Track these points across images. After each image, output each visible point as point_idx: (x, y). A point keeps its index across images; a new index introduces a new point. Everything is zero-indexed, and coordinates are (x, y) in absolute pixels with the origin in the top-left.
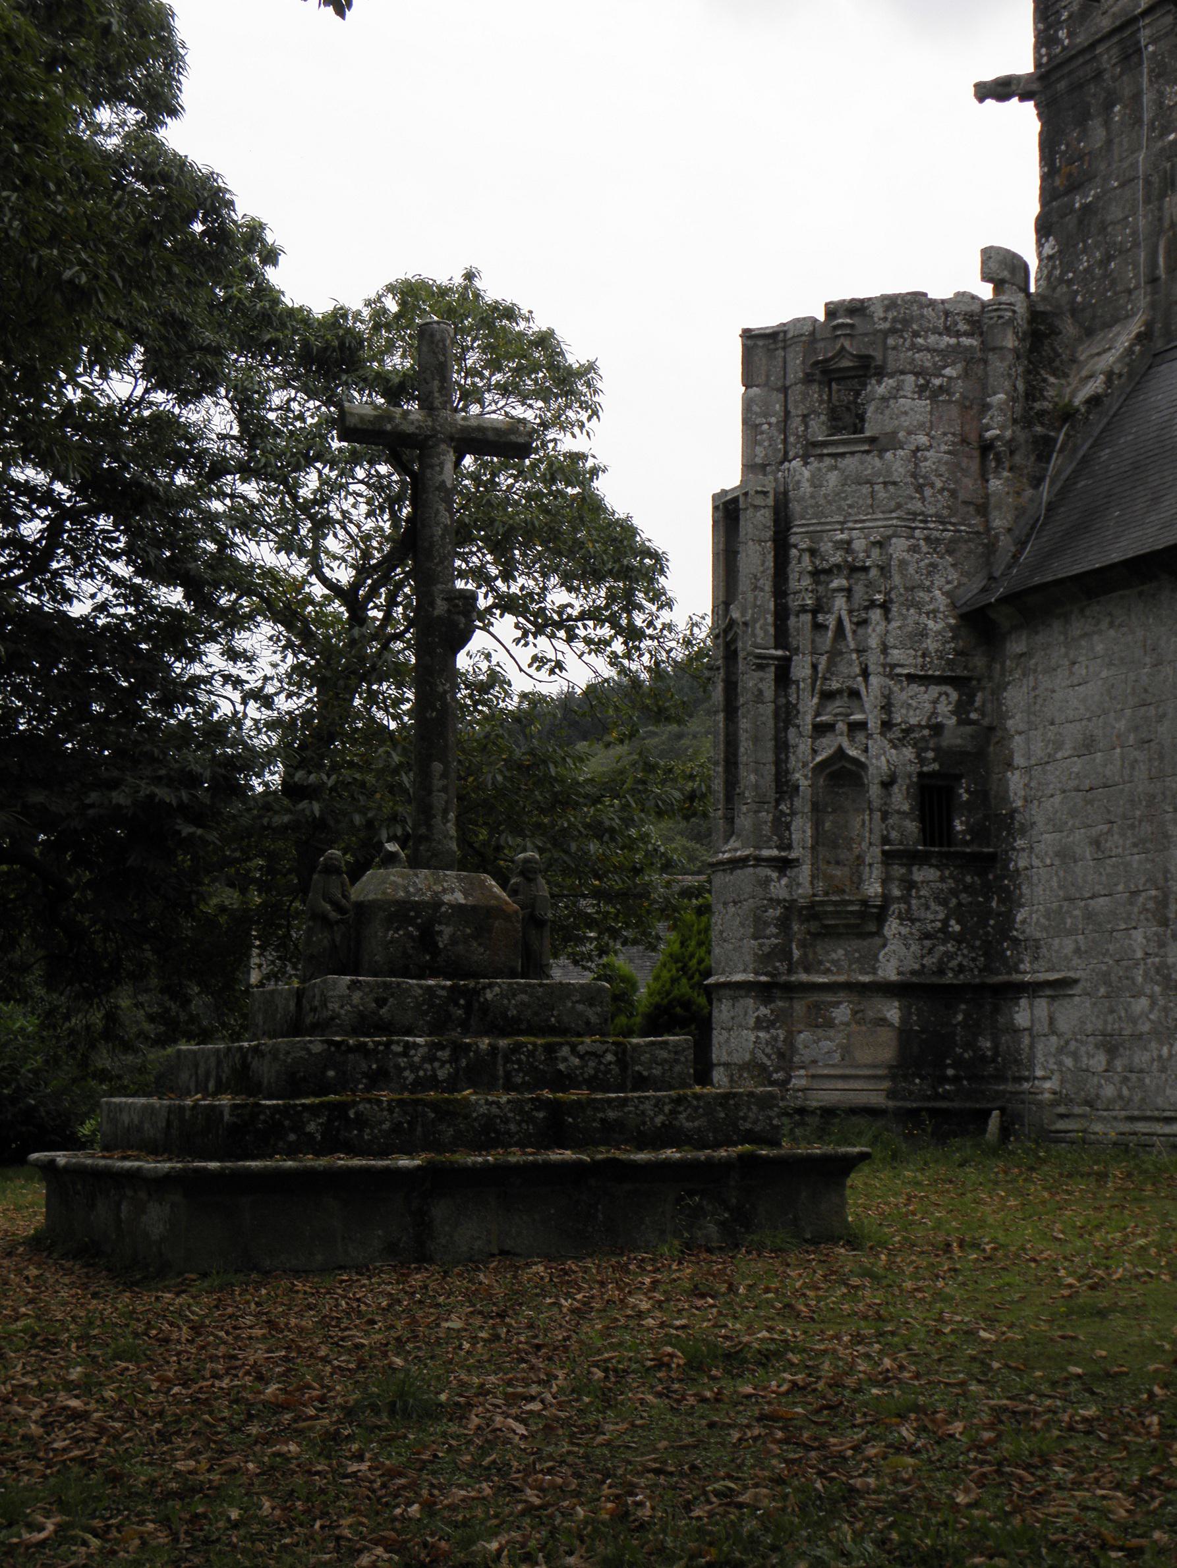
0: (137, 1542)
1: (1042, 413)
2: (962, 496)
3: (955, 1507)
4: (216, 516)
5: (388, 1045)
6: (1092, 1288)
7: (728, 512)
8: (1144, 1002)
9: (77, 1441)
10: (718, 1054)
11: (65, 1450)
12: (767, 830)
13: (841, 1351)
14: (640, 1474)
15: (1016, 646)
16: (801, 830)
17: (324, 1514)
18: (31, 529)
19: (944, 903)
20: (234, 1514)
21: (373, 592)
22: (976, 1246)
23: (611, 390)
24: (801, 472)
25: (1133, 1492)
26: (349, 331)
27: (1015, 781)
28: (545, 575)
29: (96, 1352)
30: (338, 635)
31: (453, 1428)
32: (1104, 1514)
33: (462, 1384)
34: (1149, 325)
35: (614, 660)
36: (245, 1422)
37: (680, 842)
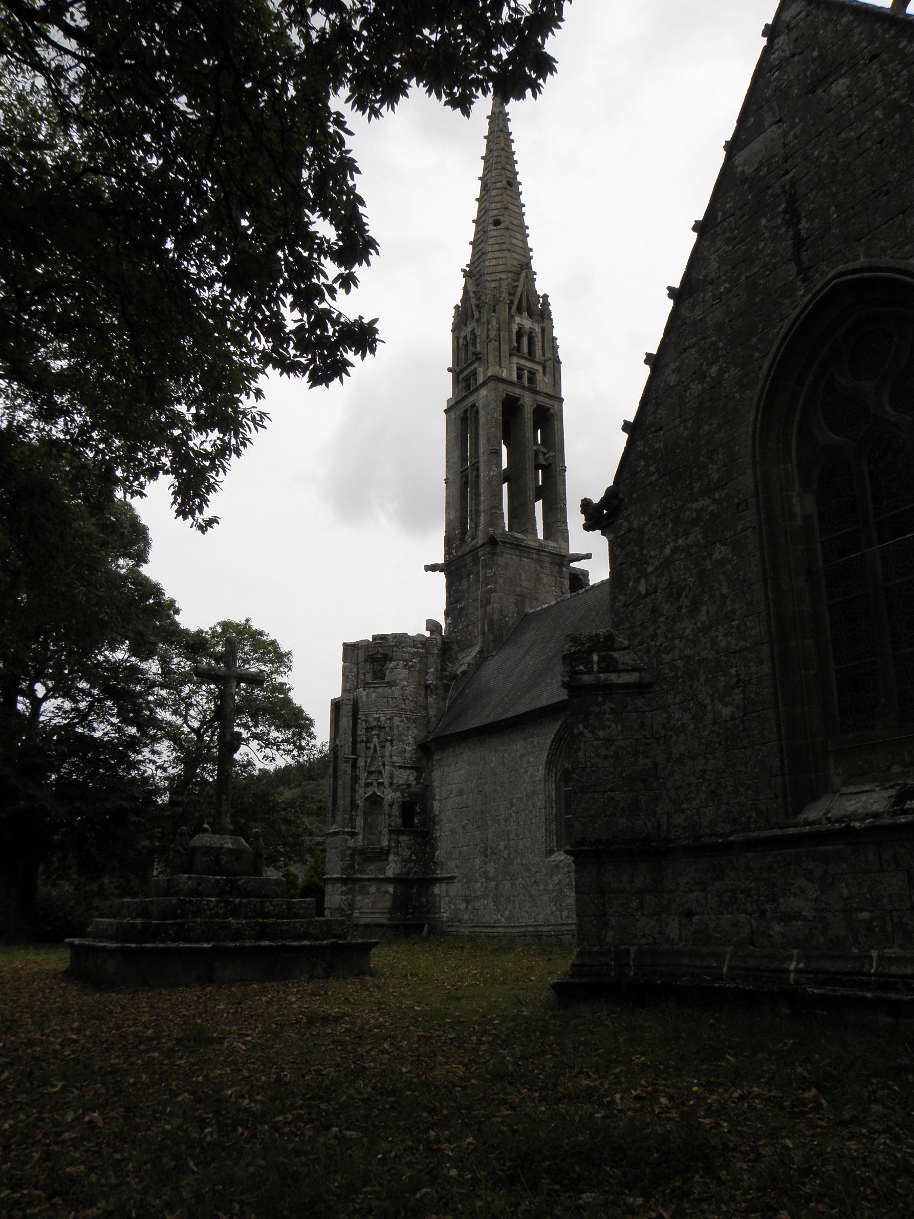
0: (93, 1092)
1: (446, 676)
2: (419, 703)
3: (401, 1073)
4: (150, 702)
5: (201, 901)
6: (456, 989)
7: (336, 706)
8: (479, 884)
9: (74, 1052)
10: (327, 904)
11: (69, 1055)
12: (347, 821)
13: (365, 1016)
14: (287, 1064)
15: (437, 757)
16: (360, 822)
17: (166, 1081)
18: (83, 705)
19: (410, 849)
20: (131, 1081)
21: (206, 731)
22: (416, 975)
23: (295, 661)
24: (362, 692)
25: (465, 1065)
26: (203, 638)
27: (436, 805)
28: (270, 726)
29: (84, 1017)
30: (192, 746)
31: (218, 1047)
32: (455, 1073)
33: (223, 1030)
34: (482, 648)
35: (294, 757)
36: (139, 1044)
37: (317, 824)
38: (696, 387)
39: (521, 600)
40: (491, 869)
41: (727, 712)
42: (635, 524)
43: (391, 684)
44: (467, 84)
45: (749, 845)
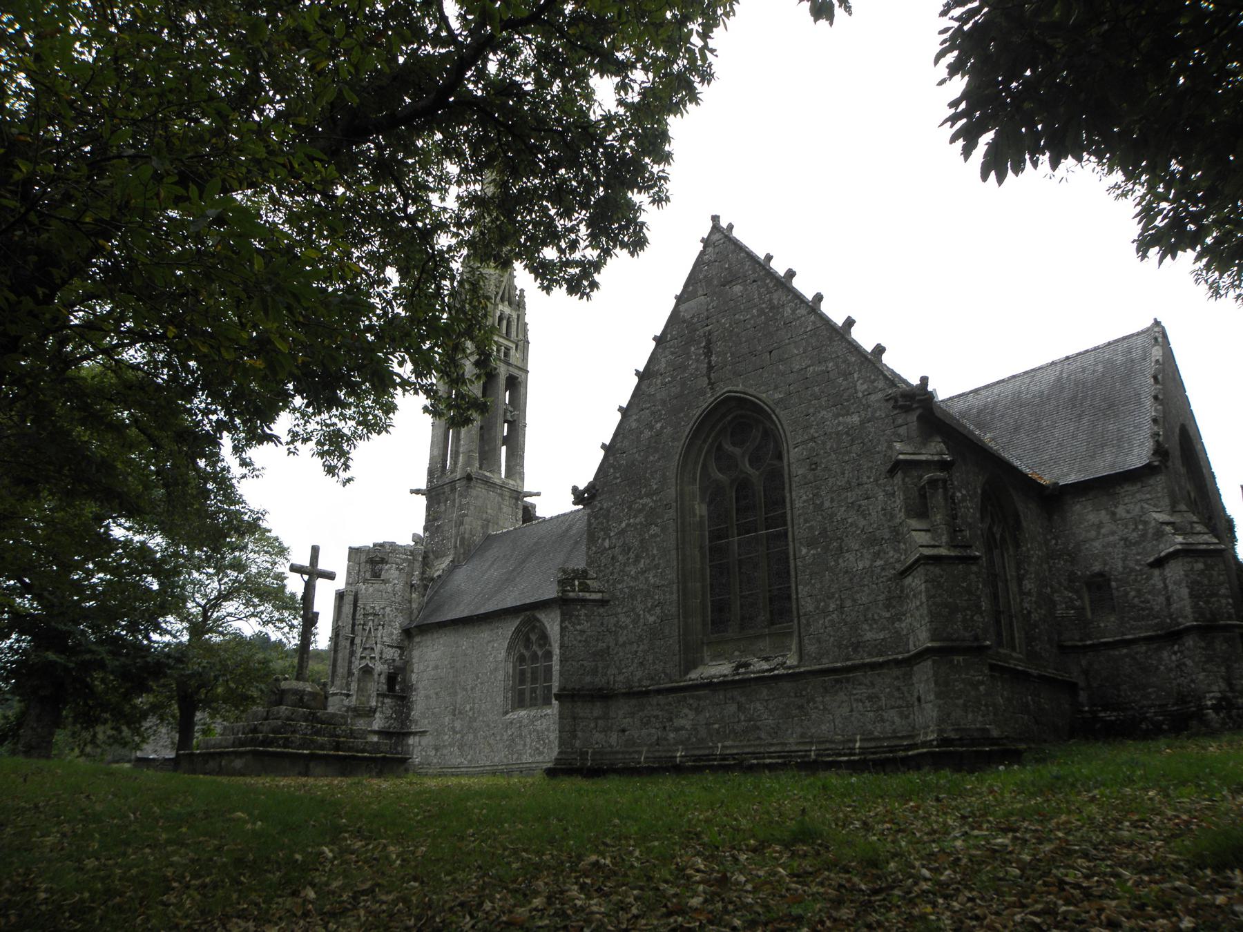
15: (417, 639)
16: (354, 686)
24: (362, 587)
27: (414, 676)
38: (647, 433)
39: (486, 523)
40: (458, 725)
41: (651, 619)
42: (605, 506)
43: (385, 582)
44: (551, 281)
45: (659, 692)
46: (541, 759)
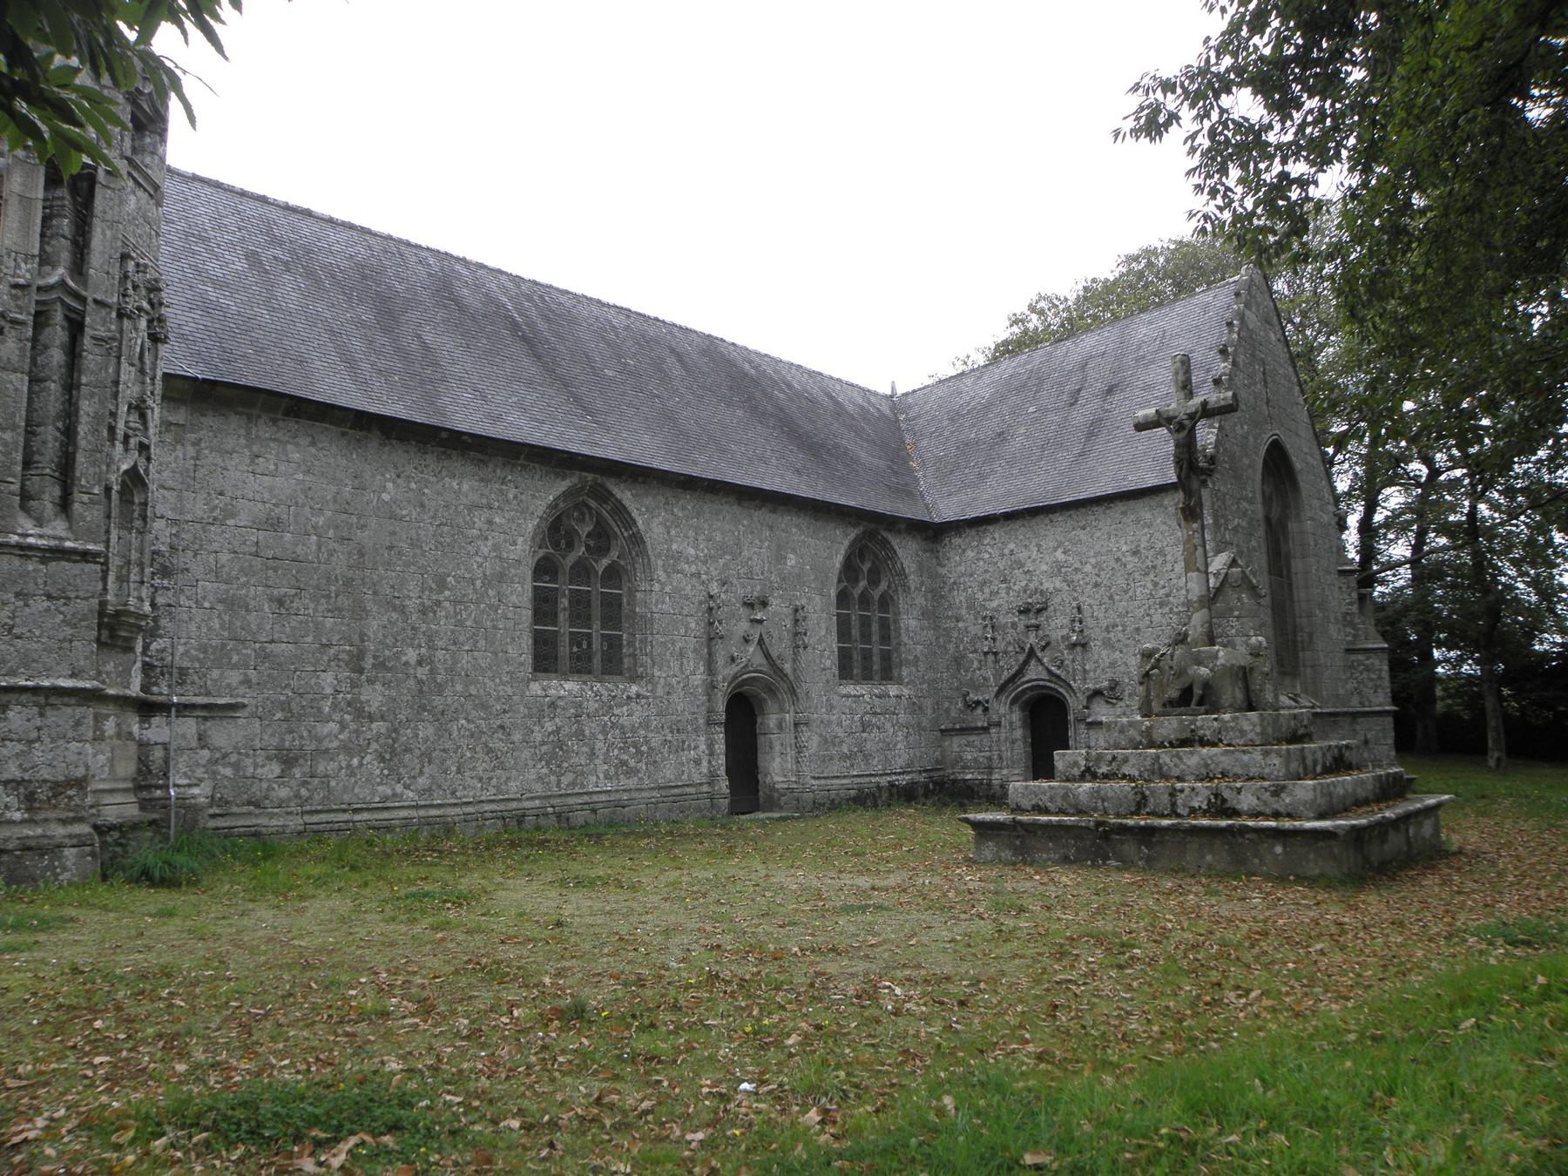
40: (374, 697)
46: (632, 783)
